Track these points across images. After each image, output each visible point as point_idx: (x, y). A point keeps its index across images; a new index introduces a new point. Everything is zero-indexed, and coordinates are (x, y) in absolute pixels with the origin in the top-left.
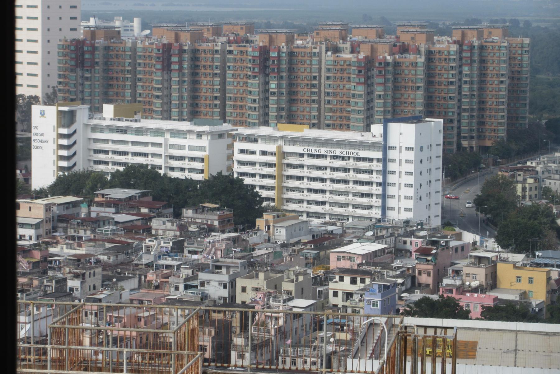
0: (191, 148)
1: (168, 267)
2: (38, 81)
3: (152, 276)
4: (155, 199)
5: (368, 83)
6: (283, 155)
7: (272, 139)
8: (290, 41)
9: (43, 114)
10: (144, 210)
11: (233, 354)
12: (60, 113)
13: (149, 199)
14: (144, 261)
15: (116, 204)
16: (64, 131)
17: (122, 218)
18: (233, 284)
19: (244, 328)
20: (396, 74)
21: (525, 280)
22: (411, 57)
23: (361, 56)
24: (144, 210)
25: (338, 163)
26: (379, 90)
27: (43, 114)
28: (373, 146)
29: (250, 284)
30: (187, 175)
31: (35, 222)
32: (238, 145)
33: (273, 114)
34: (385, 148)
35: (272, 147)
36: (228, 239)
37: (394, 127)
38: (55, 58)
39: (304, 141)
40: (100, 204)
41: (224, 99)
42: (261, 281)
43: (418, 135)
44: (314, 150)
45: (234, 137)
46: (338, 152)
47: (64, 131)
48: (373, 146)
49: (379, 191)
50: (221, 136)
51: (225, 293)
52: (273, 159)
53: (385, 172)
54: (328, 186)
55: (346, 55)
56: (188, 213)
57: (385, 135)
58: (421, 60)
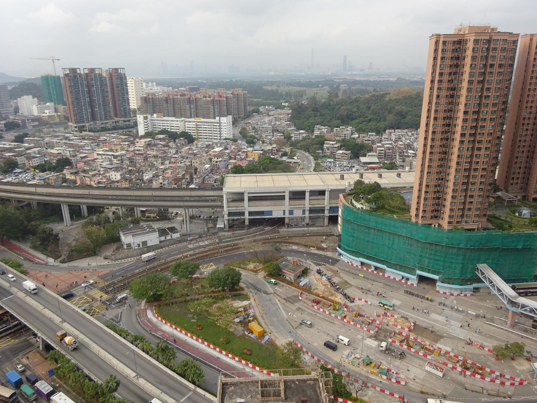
0: (176, 124)
1: (176, 157)
2: (135, 104)
3: (173, 160)
4: (169, 137)
5: (214, 105)
6: (197, 125)
7: (194, 122)
8: (195, 96)
9: (140, 117)
10: (167, 141)
11: (194, 180)
12: (144, 117)
13: (167, 137)
14: (170, 156)
15: (160, 139)
16: (145, 121)
17: (162, 143)
18: (191, 162)
19: (195, 173)
20: (220, 102)
21: (253, 155)
22: (223, 99)
23: (211, 99)
24: (167, 141)
25: (209, 127)
26: (216, 107)
27: (140, 117)
28: (217, 123)
29: (195, 161)
30: (175, 130)
31: (142, 146)
32: (186, 123)
33: (193, 115)
34: (220, 123)
35: (194, 124)
36: (188, 149)
37: (221, 118)
38: (139, 101)
39: (201, 122)
40: (156, 139)
41: (181, 109)
42: (197, 160)
43: (227, 120)
44: (204, 124)
45: (185, 122)
46: (209, 124)
47: (145, 121)
48: (217, 123)
49: (219, 135)
50: (182, 121)
51: (190, 164)
52: (195, 126)
53: (220, 128)
54: (207, 132)
55: (208, 99)
56: (177, 141)
57: (219, 120)
58: (225, 99)
